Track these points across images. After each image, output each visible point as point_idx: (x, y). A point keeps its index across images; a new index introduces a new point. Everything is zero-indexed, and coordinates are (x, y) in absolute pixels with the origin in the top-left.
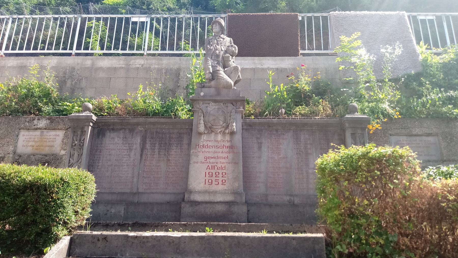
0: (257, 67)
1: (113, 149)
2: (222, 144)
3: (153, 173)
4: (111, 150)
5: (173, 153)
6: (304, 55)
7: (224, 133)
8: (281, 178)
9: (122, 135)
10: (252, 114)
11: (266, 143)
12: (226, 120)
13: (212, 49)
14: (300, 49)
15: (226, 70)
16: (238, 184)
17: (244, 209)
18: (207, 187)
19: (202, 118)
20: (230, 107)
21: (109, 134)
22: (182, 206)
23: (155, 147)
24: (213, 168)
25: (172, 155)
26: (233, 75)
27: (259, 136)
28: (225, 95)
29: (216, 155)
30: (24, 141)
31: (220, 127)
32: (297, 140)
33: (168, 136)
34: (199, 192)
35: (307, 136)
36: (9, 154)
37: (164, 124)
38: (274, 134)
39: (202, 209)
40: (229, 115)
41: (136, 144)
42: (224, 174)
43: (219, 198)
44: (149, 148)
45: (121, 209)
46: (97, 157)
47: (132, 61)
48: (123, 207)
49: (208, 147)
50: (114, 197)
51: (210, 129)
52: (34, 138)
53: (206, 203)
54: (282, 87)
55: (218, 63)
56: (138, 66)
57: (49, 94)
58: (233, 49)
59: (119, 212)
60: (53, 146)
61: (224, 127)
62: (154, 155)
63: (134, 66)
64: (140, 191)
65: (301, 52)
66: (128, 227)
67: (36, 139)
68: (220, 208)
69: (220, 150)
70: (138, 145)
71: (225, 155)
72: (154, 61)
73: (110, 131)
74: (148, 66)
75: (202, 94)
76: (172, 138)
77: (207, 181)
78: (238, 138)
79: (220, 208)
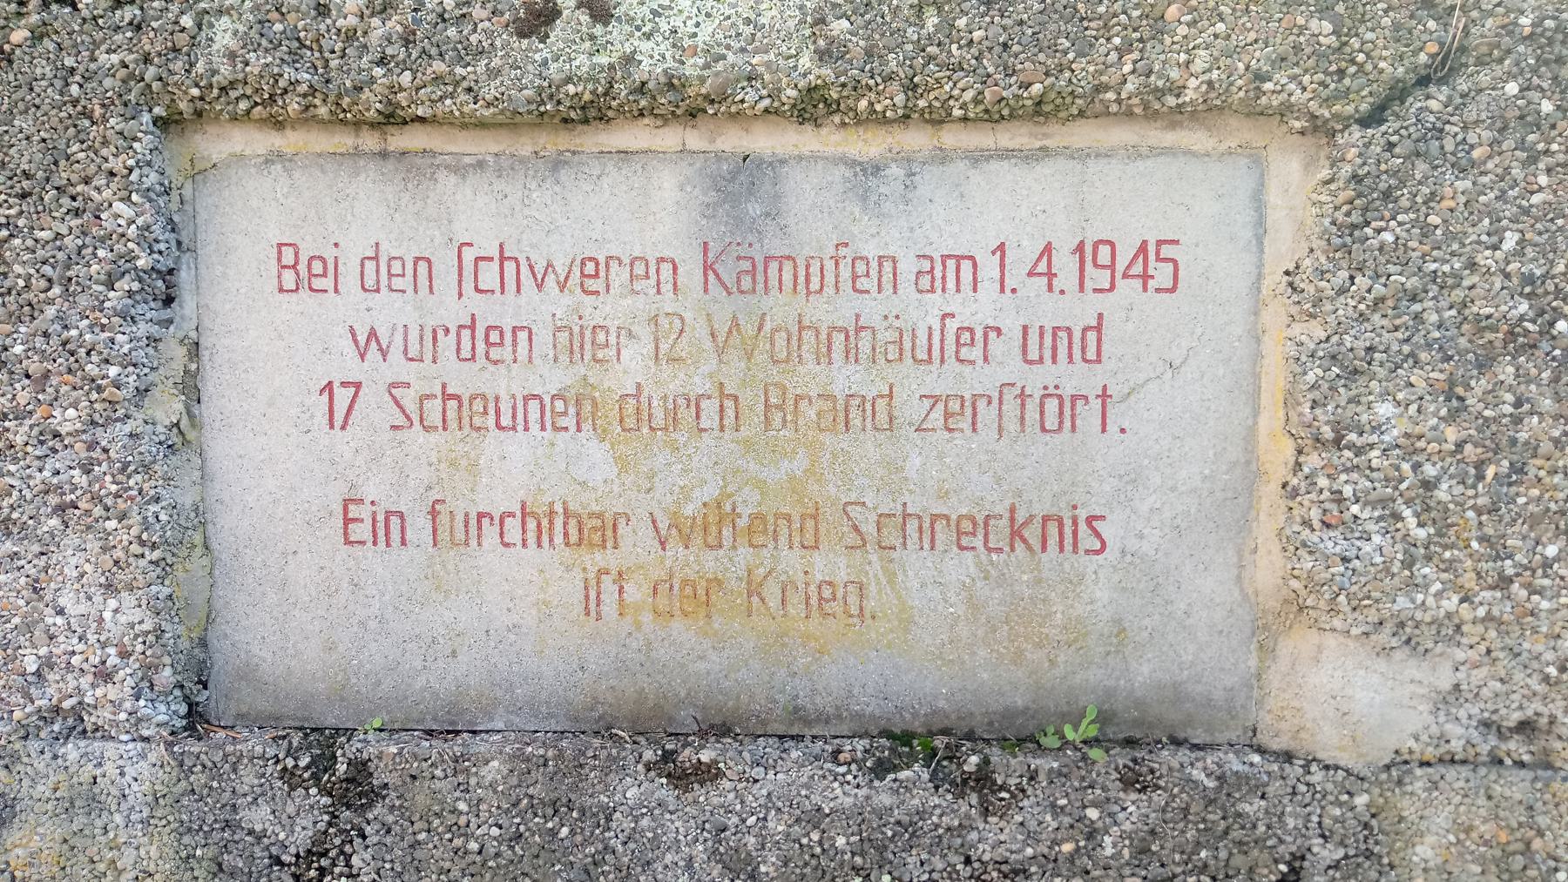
30: (338, 403)
36: (74, 723)
52: (581, 342)
57: (796, 709)
60: (1070, 530)
67: (633, 366)
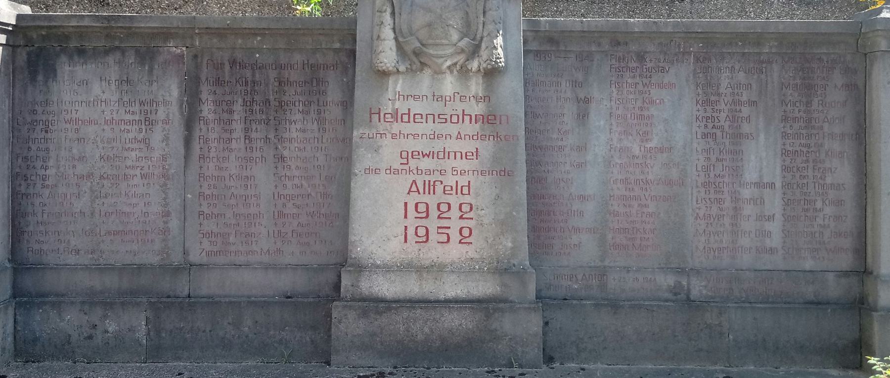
1: (90, 122)
2: (459, 107)
3: (233, 202)
4: (83, 122)
5: (294, 135)
7: (464, 72)
8: (650, 215)
9: (113, 72)
11: (604, 100)
16: (513, 242)
17: (534, 323)
18: (412, 251)
19: (387, 18)
21: (67, 68)
22: (335, 314)
23: (231, 112)
24: (430, 187)
25: (290, 140)
27: (580, 76)
29: (438, 146)
31: (450, 51)
32: (708, 95)
33: (273, 74)
34: (387, 269)
37: (256, 35)
38: (631, 70)
39: (397, 324)
40: (481, 8)
41: (166, 103)
42: (466, 208)
43: (452, 288)
44: (211, 116)
46: (39, 149)
48: (143, 316)
49: (412, 117)
50: (111, 282)
51: (415, 58)
53: (412, 303)
59: (131, 330)
61: (463, 51)
68: (456, 322)
69: (453, 129)
70: (174, 109)
71: (469, 146)
73: (71, 57)
76: (289, 83)
77: (411, 232)
78: (511, 88)
79: (457, 323)
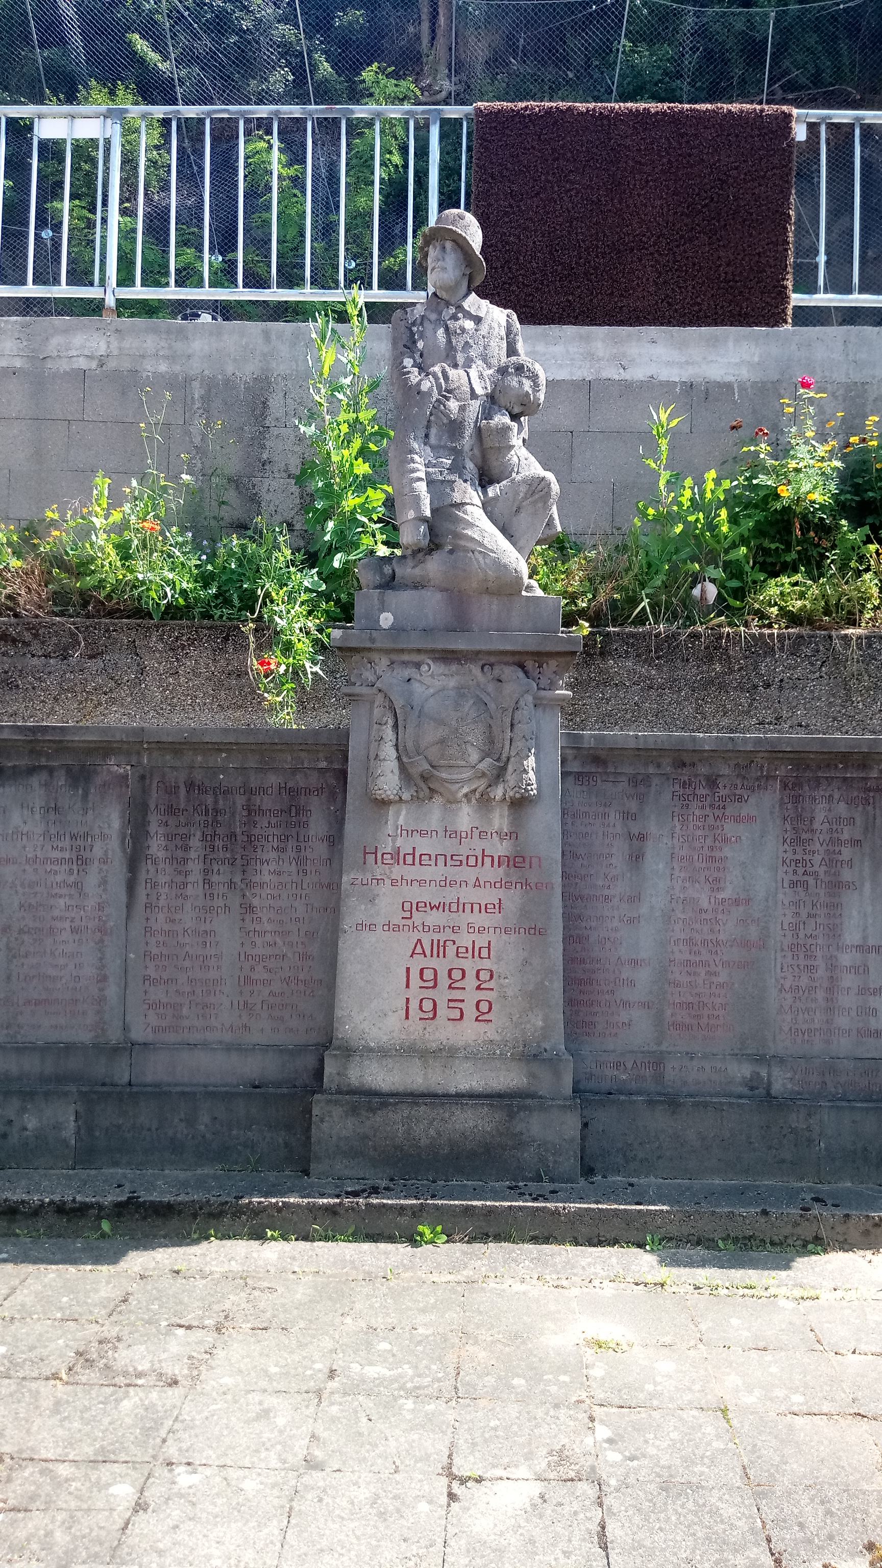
0: (605, 374)
2: (478, 845)
3: (187, 963)
5: (266, 878)
6: (806, 317)
7: (484, 801)
8: (722, 986)
10: (582, 613)
12: (492, 742)
13: (429, 393)
14: (789, 284)
15: (496, 498)
16: (545, 1020)
18: (415, 1029)
19: (389, 733)
20: (510, 672)
23: (186, 848)
24: (440, 949)
25: (262, 885)
26: (522, 522)
28: (490, 629)
29: (450, 895)
31: (467, 774)
32: (798, 829)
33: (240, 800)
34: (383, 1053)
35: (842, 809)
37: (221, 750)
39: (394, 1124)
42: (484, 976)
43: (466, 1078)
44: (161, 854)
45: (64, 1117)
47: (56, 341)
50: (32, 1065)
51: (423, 783)
54: (710, 485)
55: (457, 468)
56: (82, 363)
58: (527, 385)
59: (57, 1127)
61: (484, 774)
62: (185, 885)
63: (64, 366)
64: (137, 1034)
65: (797, 299)
66: (99, 1218)
68: (470, 1122)
69: (469, 874)
70: (114, 844)
71: (489, 896)
72: (150, 343)
74: (126, 365)
75: (386, 620)
77: (414, 1005)
78: (545, 823)
